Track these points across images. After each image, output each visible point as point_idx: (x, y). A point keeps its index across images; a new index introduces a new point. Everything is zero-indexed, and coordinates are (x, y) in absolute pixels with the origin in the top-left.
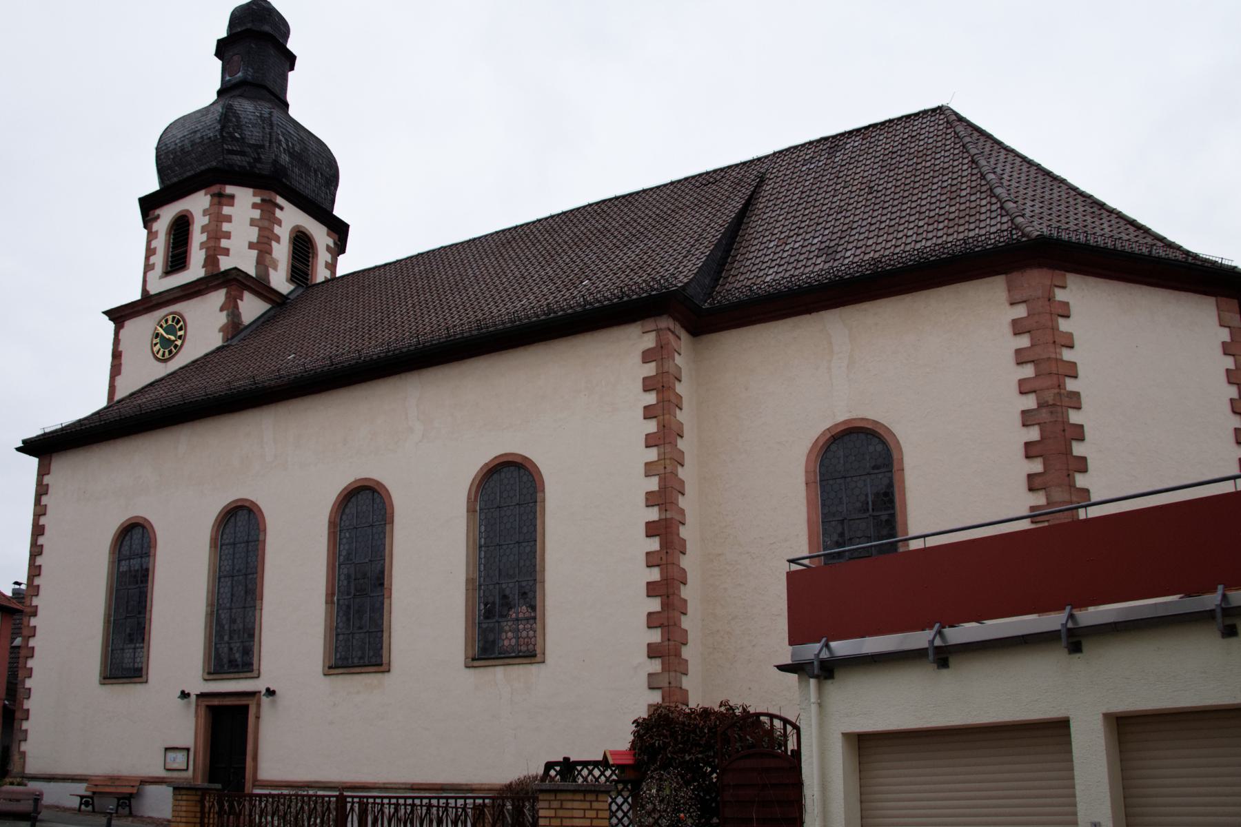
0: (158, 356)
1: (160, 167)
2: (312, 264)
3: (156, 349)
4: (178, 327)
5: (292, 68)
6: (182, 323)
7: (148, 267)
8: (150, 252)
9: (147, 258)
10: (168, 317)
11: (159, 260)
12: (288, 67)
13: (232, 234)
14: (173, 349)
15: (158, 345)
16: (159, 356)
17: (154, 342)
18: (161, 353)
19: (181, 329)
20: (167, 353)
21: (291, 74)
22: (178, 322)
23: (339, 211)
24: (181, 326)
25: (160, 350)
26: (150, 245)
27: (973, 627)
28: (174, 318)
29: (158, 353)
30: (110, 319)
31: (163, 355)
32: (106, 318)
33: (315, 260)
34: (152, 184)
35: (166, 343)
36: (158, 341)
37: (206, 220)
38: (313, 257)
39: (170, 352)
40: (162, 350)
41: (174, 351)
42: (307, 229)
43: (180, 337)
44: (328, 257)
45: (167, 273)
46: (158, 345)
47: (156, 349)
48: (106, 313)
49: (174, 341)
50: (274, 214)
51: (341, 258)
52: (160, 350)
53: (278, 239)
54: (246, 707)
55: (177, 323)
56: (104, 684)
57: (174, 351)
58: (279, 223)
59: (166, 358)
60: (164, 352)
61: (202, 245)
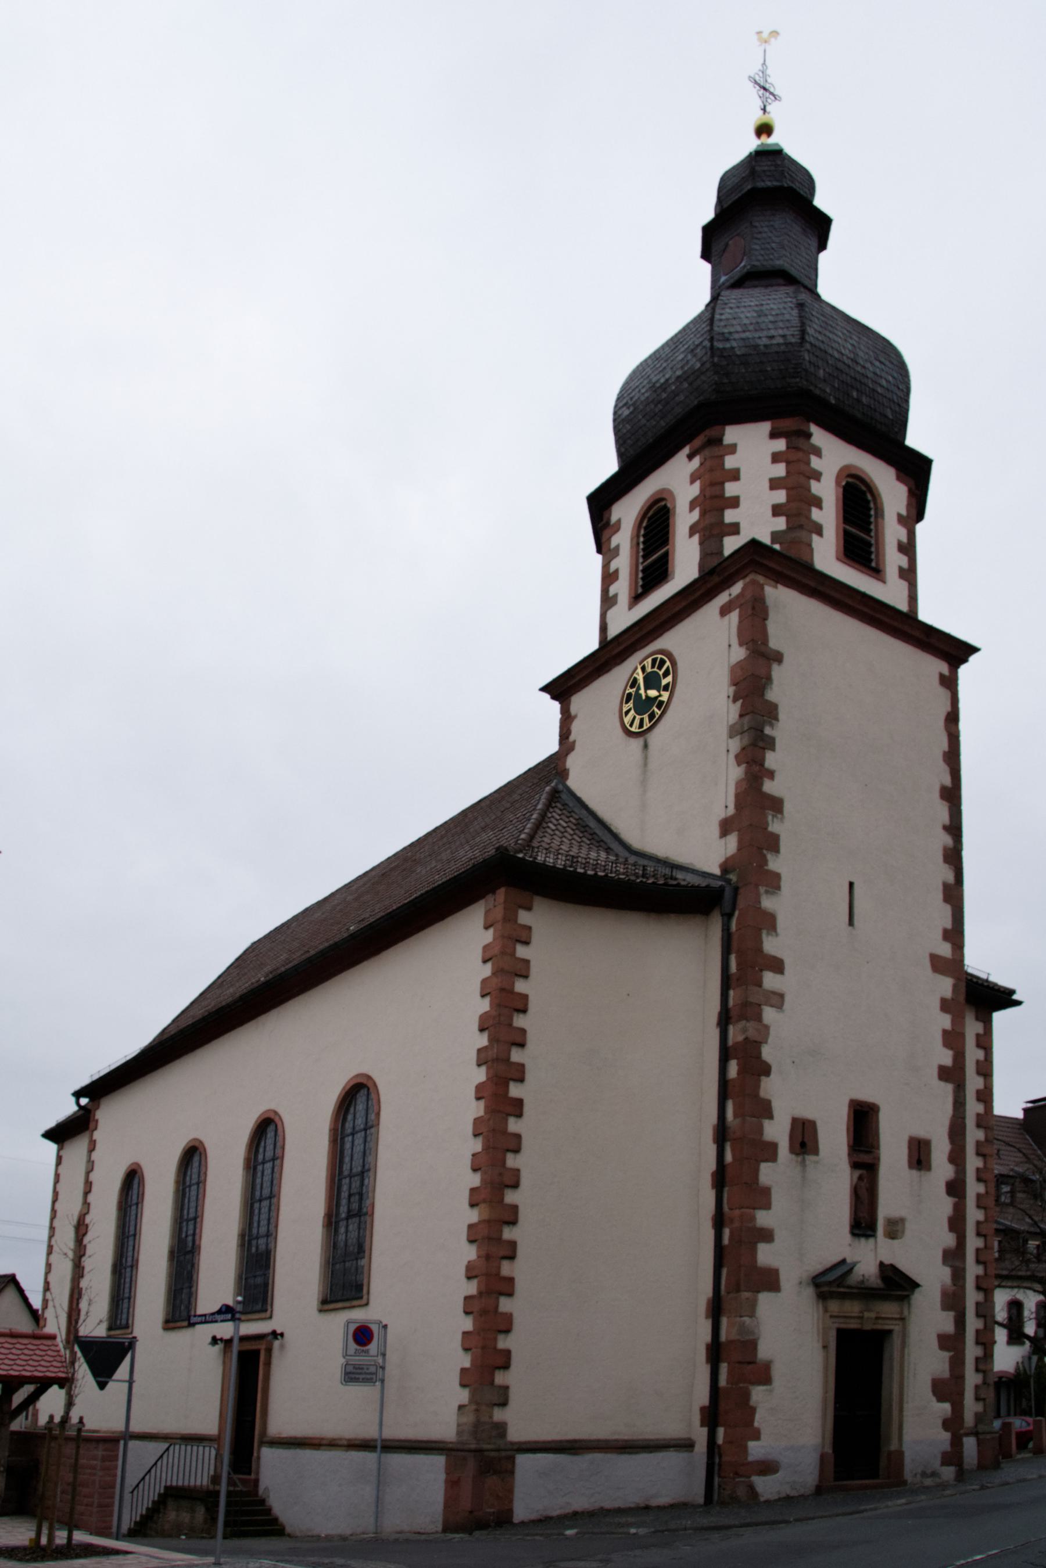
0: (633, 729)
1: (623, 450)
2: (876, 526)
3: (627, 720)
4: (661, 673)
5: (822, 246)
6: (668, 663)
7: (608, 601)
8: (609, 577)
9: (605, 591)
10: (645, 662)
11: (622, 588)
12: (814, 244)
13: (742, 526)
14: (656, 710)
15: (632, 712)
16: (634, 729)
17: (625, 710)
18: (637, 722)
19: (666, 674)
20: (646, 720)
21: (823, 257)
22: (662, 662)
23: (915, 439)
24: (667, 670)
25: (634, 718)
26: (609, 568)
27: (727, 1275)
28: (654, 661)
29: (631, 725)
30: (554, 698)
31: (641, 725)
32: (546, 696)
33: (880, 520)
34: (608, 465)
35: (643, 705)
36: (632, 706)
37: (695, 490)
38: (876, 517)
39: (652, 717)
40: (638, 717)
41: (658, 712)
42: (866, 474)
43: (666, 688)
44: (902, 534)
45: (636, 598)
46: (632, 712)
47: (627, 720)
48: (545, 689)
49: (657, 697)
50: (809, 490)
51: (920, 528)
52: (634, 718)
53: (818, 530)
54: (257, 1353)
55: (660, 668)
56: (173, 1329)
57: (658, 712)
58: (817, 476)
59: (645, 728)
60: (642, 720)
61: (693, 530)
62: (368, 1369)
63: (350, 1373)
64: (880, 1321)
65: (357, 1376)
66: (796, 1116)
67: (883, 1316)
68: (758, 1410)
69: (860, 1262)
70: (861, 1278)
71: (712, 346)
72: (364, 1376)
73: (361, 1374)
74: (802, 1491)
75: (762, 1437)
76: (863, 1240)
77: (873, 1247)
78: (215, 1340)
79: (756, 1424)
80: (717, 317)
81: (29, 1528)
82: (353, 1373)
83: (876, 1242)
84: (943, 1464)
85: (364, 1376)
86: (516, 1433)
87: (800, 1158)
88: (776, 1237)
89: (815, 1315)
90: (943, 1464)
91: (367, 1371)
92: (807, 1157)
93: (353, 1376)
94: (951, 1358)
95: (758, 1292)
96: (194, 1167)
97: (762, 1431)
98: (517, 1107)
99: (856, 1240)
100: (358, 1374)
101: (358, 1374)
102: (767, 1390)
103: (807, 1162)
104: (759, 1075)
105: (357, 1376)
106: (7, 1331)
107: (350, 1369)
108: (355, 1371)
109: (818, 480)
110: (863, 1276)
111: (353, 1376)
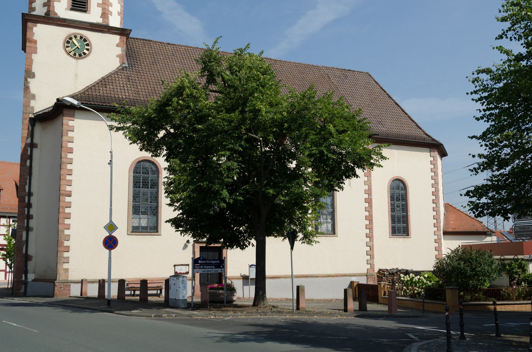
62: (528, 228)
63: (518, 232)
65: (522, 233)
71: (462, 332)
72: (527, 233)
73: (524, 231)
78: (481, 103)
80: (326, 233)
81: (115, 124)
82: (520, 232)
85: (527, 233)
86: (70, 278)
91: (528, 230)
93: (520, 233)
98: (366, 218)
100: (522, 232)
101: (522, 232)
105: (522, 233)
107: (518, 229)
108: (520, 230)
109: (98, 4)
111: (520, 233)
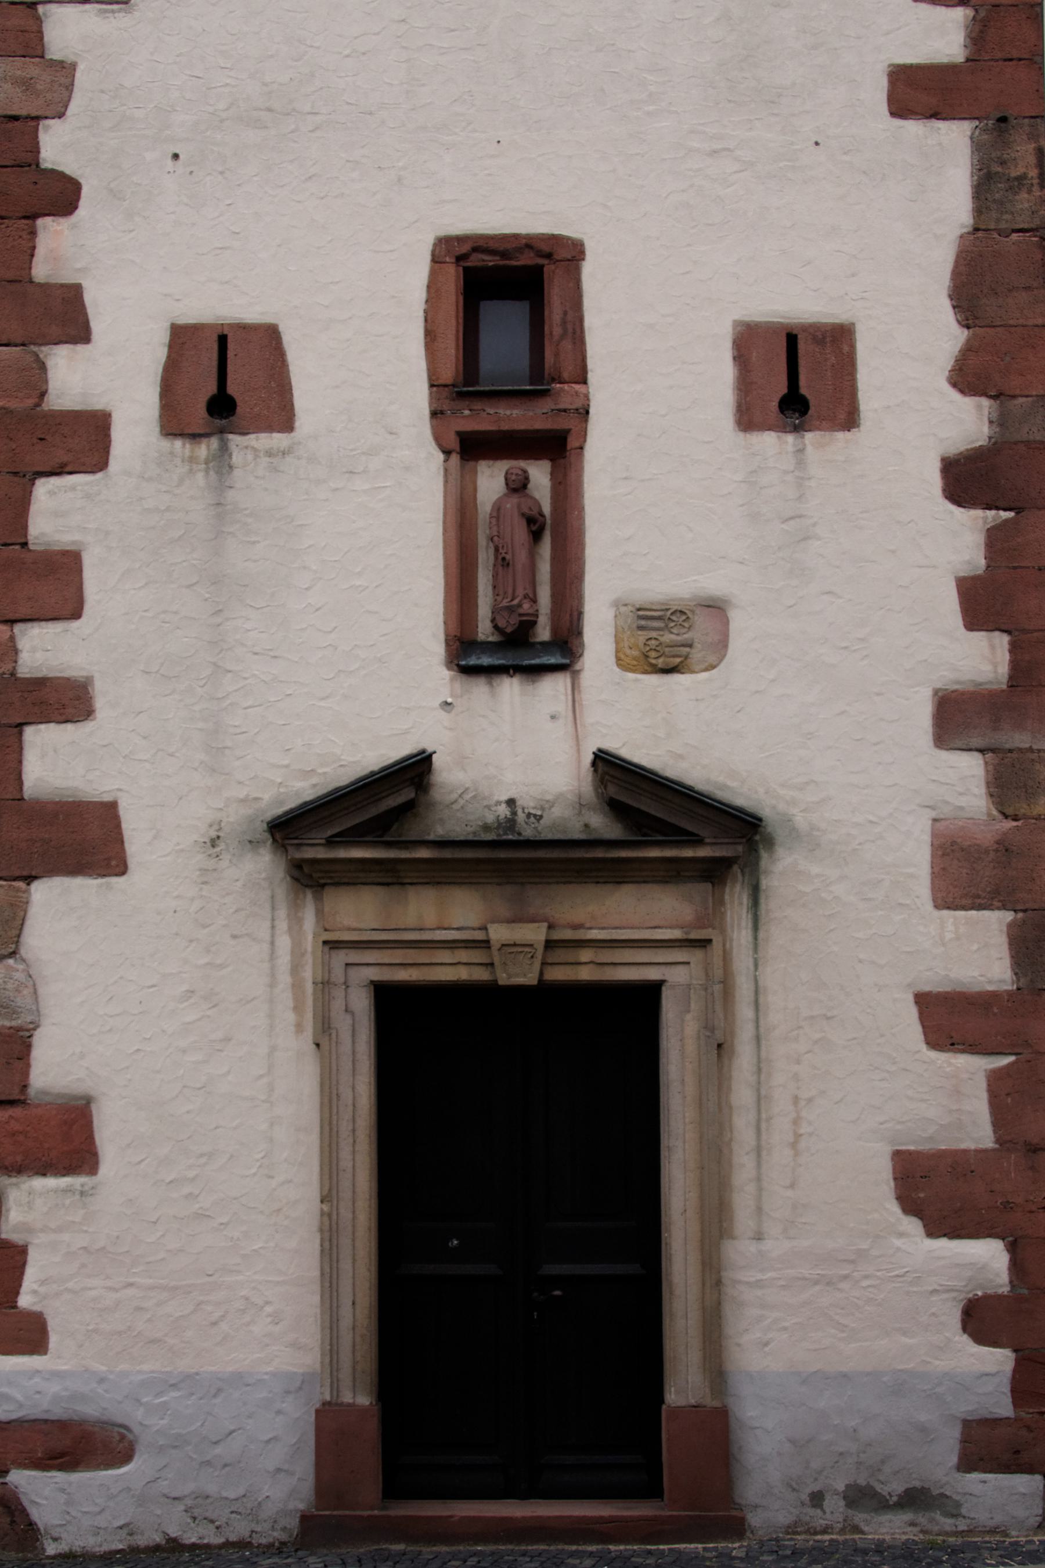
64: (560, 955)
66: (182, 321)
67: (595, 934)
68: (33, 1255)
69: (435, 752)
70: (503, 811)
74: (239, 1530)
75: (53, 1340)
76: (510, 687)
77: (562, 706)
79: (25, 1301)
83: (575, 687)
84: (969, 1463)
87: (204, 449)
88: (100, 703)
89: (284, 942)
90: (969, 1463)
92: (234, 439)
94: (996, 1081)
95: (30, 879)
96: (696, 832)
97: (52, 1325)
99: (479, 687)
102: (68, 1190)
103: (237, 458)
104: (34, 217)
106: (512, 943)
110: (511, 802)
